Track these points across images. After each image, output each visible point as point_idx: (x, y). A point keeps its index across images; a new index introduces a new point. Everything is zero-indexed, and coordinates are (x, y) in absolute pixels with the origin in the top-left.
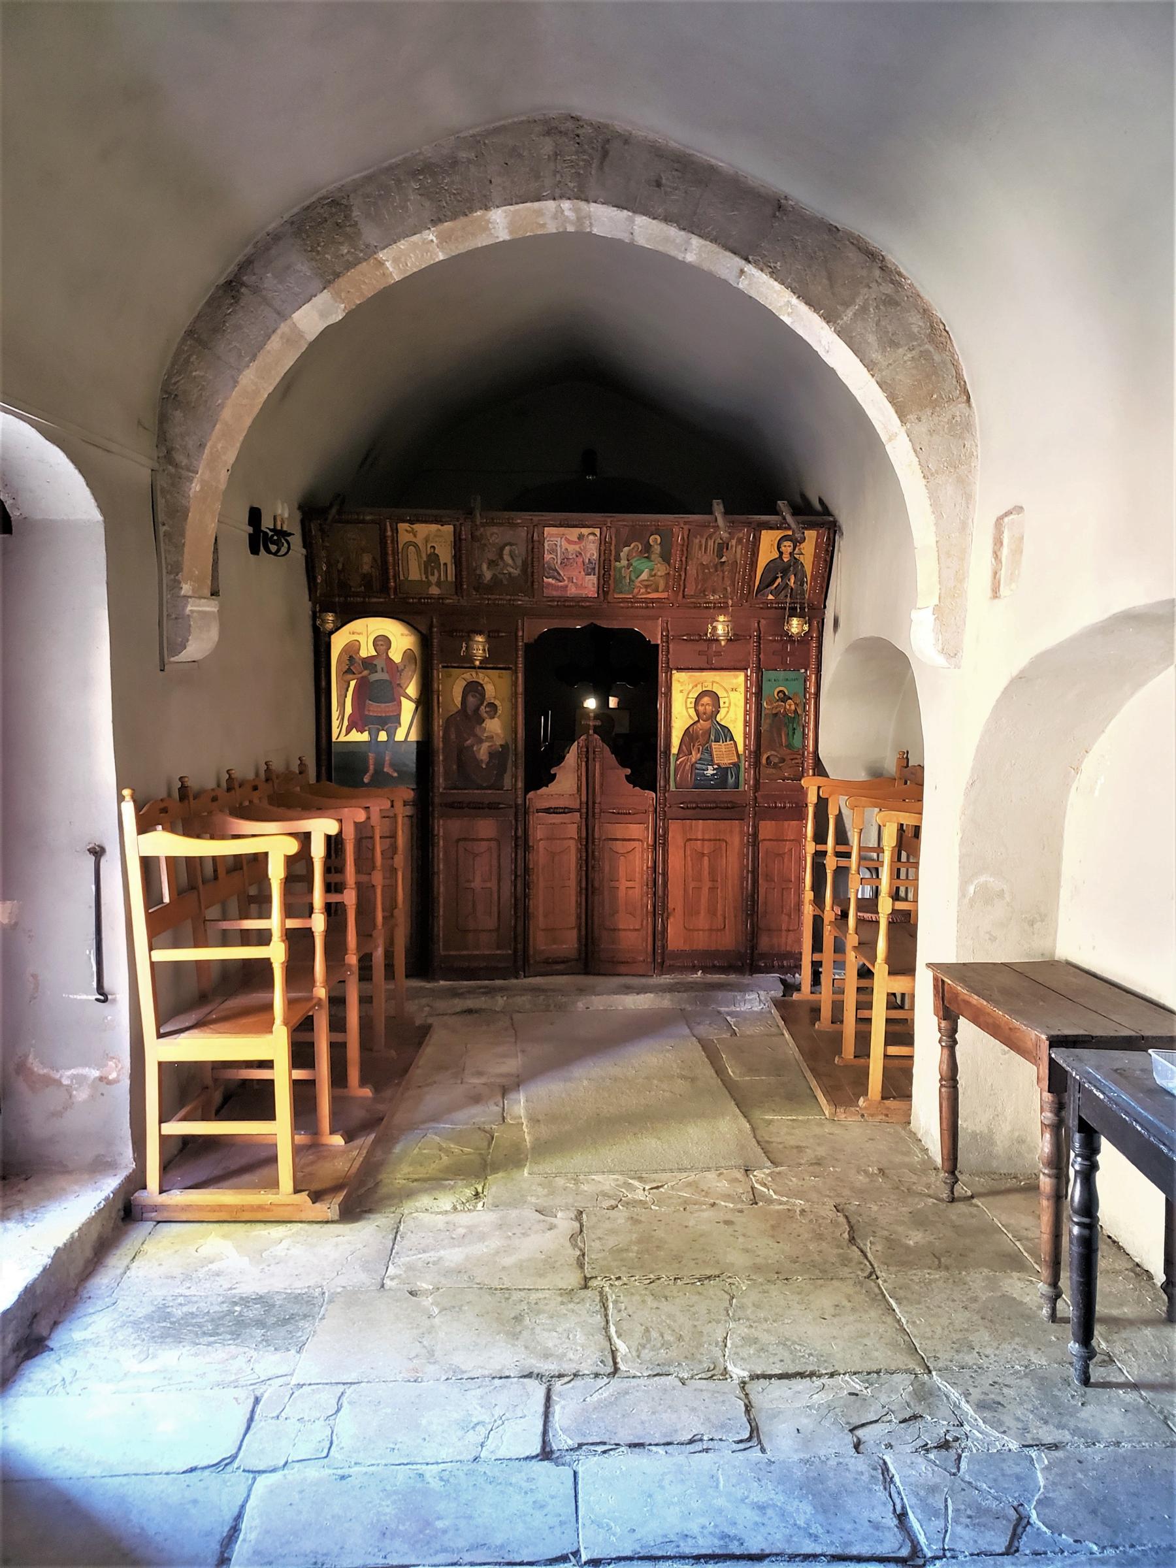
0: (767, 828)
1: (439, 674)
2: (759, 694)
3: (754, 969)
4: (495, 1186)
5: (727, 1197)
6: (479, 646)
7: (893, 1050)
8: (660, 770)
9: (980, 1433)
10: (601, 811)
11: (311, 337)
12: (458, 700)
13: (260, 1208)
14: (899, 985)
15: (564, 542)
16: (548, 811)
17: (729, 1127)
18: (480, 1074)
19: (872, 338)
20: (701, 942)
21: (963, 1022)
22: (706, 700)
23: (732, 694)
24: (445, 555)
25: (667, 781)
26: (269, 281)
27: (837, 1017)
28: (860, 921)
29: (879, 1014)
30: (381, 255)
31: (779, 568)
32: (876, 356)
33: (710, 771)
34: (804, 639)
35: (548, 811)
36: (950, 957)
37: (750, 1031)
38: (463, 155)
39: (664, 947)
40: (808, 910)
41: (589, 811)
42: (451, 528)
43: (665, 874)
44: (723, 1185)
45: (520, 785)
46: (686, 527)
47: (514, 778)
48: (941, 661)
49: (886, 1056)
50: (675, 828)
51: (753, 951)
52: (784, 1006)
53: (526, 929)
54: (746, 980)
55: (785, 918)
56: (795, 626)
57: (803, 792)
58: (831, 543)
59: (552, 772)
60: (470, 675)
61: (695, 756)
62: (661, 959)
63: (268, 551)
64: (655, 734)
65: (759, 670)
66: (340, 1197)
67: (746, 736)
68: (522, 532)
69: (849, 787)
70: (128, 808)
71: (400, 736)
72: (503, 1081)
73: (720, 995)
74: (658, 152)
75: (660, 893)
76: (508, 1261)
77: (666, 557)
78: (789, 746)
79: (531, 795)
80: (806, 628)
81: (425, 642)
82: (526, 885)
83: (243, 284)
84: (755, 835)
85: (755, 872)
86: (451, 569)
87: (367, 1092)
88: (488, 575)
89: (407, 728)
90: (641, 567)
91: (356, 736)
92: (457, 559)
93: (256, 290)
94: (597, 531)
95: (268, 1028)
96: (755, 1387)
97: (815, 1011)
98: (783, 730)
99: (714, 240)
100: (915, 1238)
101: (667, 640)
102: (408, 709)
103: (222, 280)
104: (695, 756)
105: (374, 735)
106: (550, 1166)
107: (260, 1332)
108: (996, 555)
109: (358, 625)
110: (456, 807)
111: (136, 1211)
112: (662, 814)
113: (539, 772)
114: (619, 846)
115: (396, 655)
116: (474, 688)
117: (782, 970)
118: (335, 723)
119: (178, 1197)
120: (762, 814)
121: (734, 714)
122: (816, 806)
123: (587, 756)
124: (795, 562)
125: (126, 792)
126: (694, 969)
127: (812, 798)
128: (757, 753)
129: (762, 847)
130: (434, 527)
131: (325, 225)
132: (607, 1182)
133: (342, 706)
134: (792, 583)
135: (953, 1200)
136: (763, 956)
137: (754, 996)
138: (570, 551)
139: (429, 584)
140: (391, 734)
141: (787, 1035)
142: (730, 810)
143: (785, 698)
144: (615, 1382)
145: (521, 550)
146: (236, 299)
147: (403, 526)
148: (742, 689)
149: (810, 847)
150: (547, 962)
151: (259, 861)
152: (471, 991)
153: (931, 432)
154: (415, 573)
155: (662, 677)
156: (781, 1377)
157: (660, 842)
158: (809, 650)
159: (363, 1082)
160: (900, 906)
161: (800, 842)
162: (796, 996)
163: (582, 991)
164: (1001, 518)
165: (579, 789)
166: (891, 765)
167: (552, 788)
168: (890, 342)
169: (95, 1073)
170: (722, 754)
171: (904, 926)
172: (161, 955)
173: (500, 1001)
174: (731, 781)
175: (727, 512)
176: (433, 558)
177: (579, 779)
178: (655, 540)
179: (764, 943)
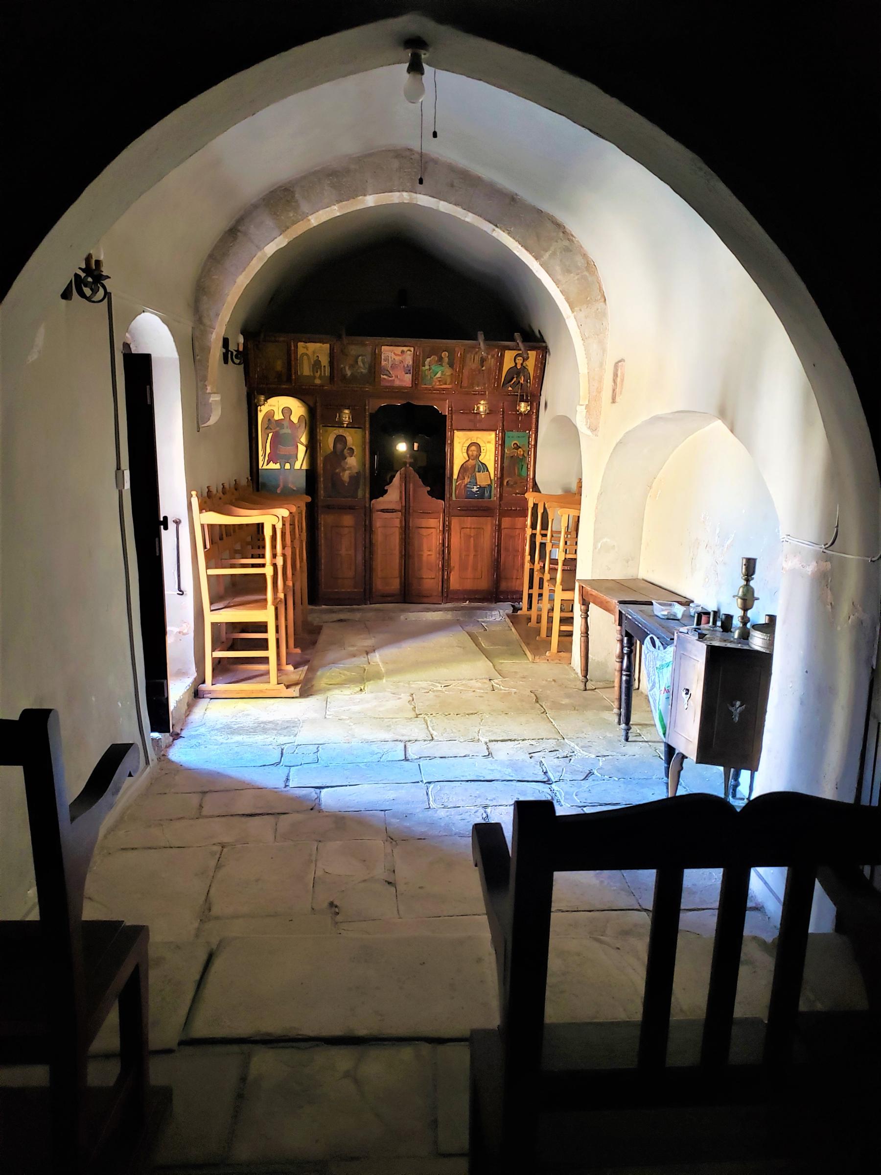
0: (506, 522)
1: (320, 430)
2: (503, 445)
3: (498, 600)
4: (369, 686)
5: (480, 689)
6: (346, 415)
7: (564, 628)
8: (447, 488)
9: (580, 753)
10: (414, 511)
11: (269, 256)
12: (331, 446)
13: (261, 691)
14: (567, 595)
15: (393, 356)
16: (383, 511)
17: (482, 665)
18: (353, 646)
19: (558, 268)
20: (469, 585)
21: (592, 606)
22: (473, 448)
23: (488, 445)
24: (325, 361)
25: (451, 495)
26: (252, 229)
27: (539, 621)
28: (550, 569)
29: (557, 615)
30: (310, 217)
31: (515, 372)
32: (560, 277)
33: (475, 489)
34: (528, 415)
35: (383, 511)
36: (588, 577)
37: (494, 628)
38: (353, 167)
39: (448, 587)
40: (527, 566)
41: (406, 511)
42: (328, 345)
43: (449, 546)
44: (479, 685)
45: (367, 495)
46: (463, 348)
47: (363, 492)
48: (589, 433)
49: (560, 631)
50: (455, 522)
51: (498, 590)
52: (514, 618)
53: (371, 578)
54: (493, 605)
55: (515, 572)
56: (523, 407)
57: (526, 501)
58: (544, 359)
59: (386, 488)
60: (341, 431)
61: (467, 480)
62: (447, 595)
63: (82, 294)
64: (444, 467)
65: (503, 431)
66: (298, 687)
67: (496, 469)
68: (369, 349)
69: (551, 497)
70: (195, 502)
71: (297, 466)
72: (367, 649)
73: (479, 612)
74: (452, 169)
75: (446, 557)
76: (381, 709)
77: (451, 365)
78: (520, 475)
79: (373, 502)
80: (529, 408)
81: (312, 412)
82: (371, 553)
83: (239, 231)
84: (500, 525)
85: (499, 545)
86: (328, 370)
87: (298, 651)
88: (349, 373)
89: (301, 462)
90: (437, 370)
91: (272, 466)
92: (331, 363)
93: (245, 234)
94: (412, 349)
95: (265, 607)
96: (491, 745)
97: (529, 619)
98: (516, 467)
99: (480, 216)
100: (565, 701)
101: (451, 412)
102: (302, 449)
103: (228, 229)
104: (467, 480)
105: (282, 466)
106: (396, 678)
107: (275, 732)
108: (615, 381)
109: (273, 401)
110: (329, 508)
111: (200, 694)
112: (447, 514)
113: (378, 491)
114: (424, 532)
115: (294, 419)
116: (340, 439)
117: (513, 600)
118: (261, 458)
119: (221, 687)
120: (504, 514)
121: (489, 457)
122: (543, 514)
123: (405, 479)
124: (524, 368)
125: (194, 493)
126: (465, 600)
127: (530, 505)
128: (501, 479)
129: (503, 532)
130: (318, 345)
131: (281, 199)
132: (424, 684)
133: (264, 448)
134: (522, 381)
135: (586, 690)
136: (503, 592)
137: (496, 612)
138: (397, 359)
139: (315, 377)
140: (292, 466)
141: (513, 629)
142: (484, 511)
143: (517, 447)
144: (432, 742)
145: (368, 359)
146: (235, 238)
147: (300, 344)
148: (494, 442)
149: (529, 531)
150: (383, 596)
151: (260, 527)
152: (341, 611)
153: (586, 317)
154: (306, 370)
155: (449, 434)
156: (502, 741)
157: (446, 529)
158: (531, 420)
159: (296, 647)
160: (568, 556)
161: (524, 530)
162: (519, 612)
163: (403, 611)
164: (617, 363)
165: (401, 498)
166: (574, 487)
167: (386, 498)
168: (567, 271)
169: (178, 630)
170: (482, 479)
171: (571, 565)
172: (212, 572)
173: (358, 616)
174: (486, 495)
175: (486, 339)
176: (317, 363)
177: (401, 492)
178: (445, 355)
179: (504, 586)
